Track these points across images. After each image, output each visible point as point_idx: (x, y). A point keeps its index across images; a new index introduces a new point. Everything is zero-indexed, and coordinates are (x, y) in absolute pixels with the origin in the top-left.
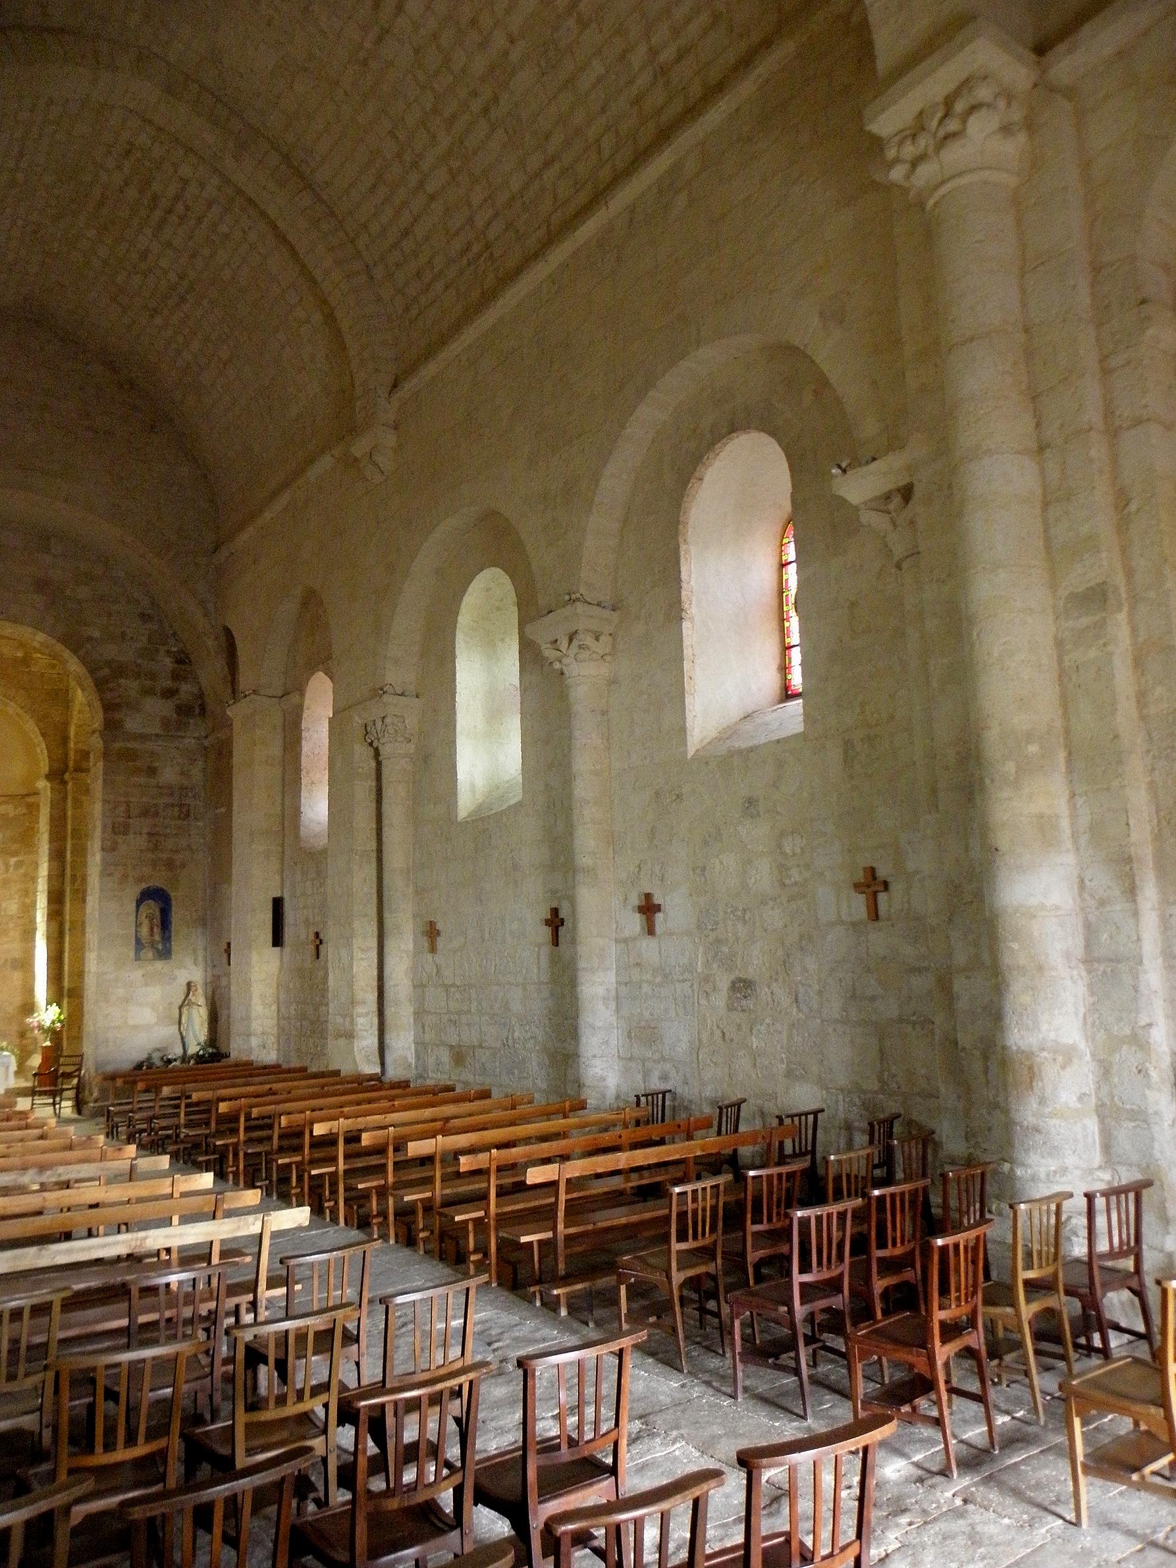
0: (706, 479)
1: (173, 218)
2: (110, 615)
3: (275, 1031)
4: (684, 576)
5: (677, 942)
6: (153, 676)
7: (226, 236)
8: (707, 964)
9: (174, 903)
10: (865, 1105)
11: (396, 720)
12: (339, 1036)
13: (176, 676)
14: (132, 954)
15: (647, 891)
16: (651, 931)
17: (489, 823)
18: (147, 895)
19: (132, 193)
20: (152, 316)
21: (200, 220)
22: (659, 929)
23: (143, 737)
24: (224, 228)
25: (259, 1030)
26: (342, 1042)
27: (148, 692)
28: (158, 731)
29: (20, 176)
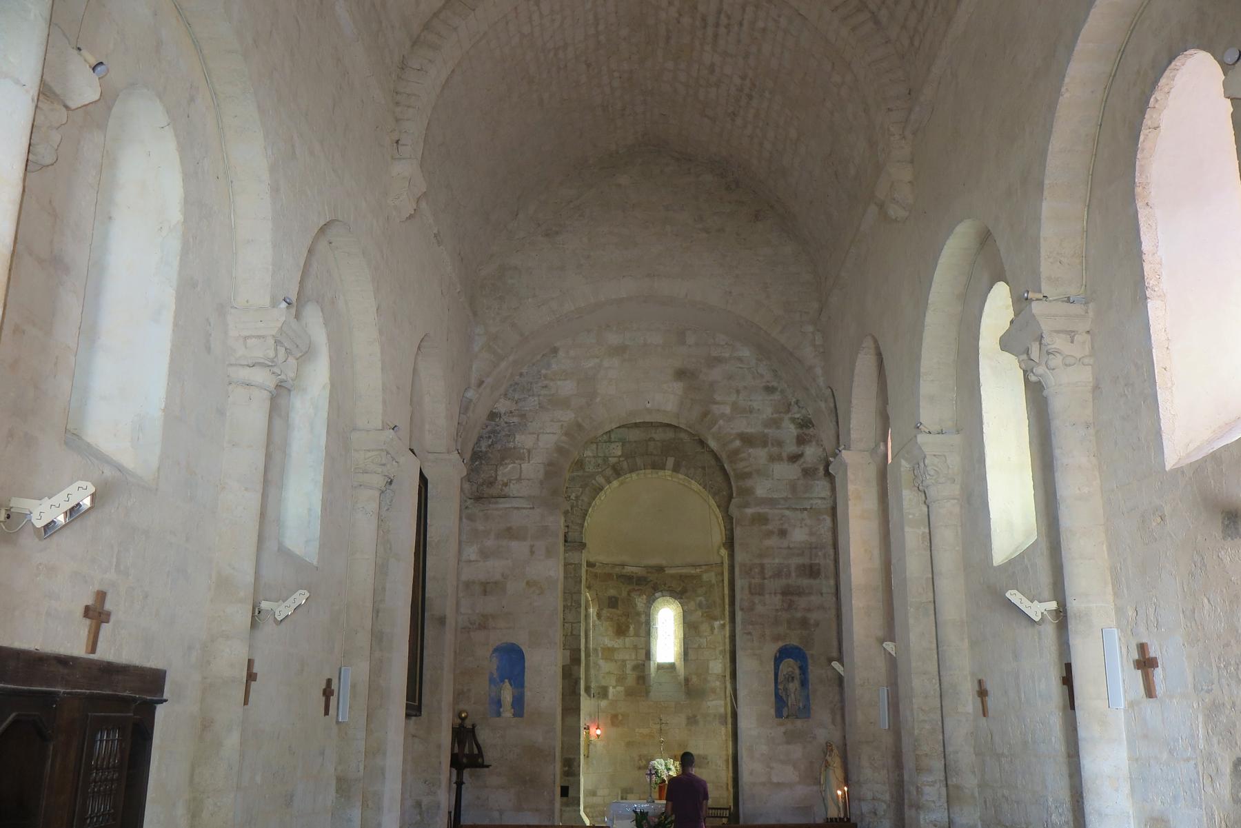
0: (1163, 126)
1: (722, 30)
2: (738, 392)
3: (887, 797)
4: (1146, 246)
5: (1179, 712)
6: (780, 444)
7: (764, 30)
8: (1208, 740)
9: (810, 661)
10: (705, 757)
11: (936, 460)
12: (911, 806)
13: (801, 441)
14: (773, 712)
15: (1144, 641)
16: (1150, 692)
17: (1017, 567)
18: (784, 654)
19: (686, 20)
20: (733, 120)
21: (741, 24)
22: (1160, 688)
23: (771, 502)
24: (760, 24)
25: (869, 795)
26: (913, 812)
27: (773, 459)
28: (784, 495)
29: (602, 38)
